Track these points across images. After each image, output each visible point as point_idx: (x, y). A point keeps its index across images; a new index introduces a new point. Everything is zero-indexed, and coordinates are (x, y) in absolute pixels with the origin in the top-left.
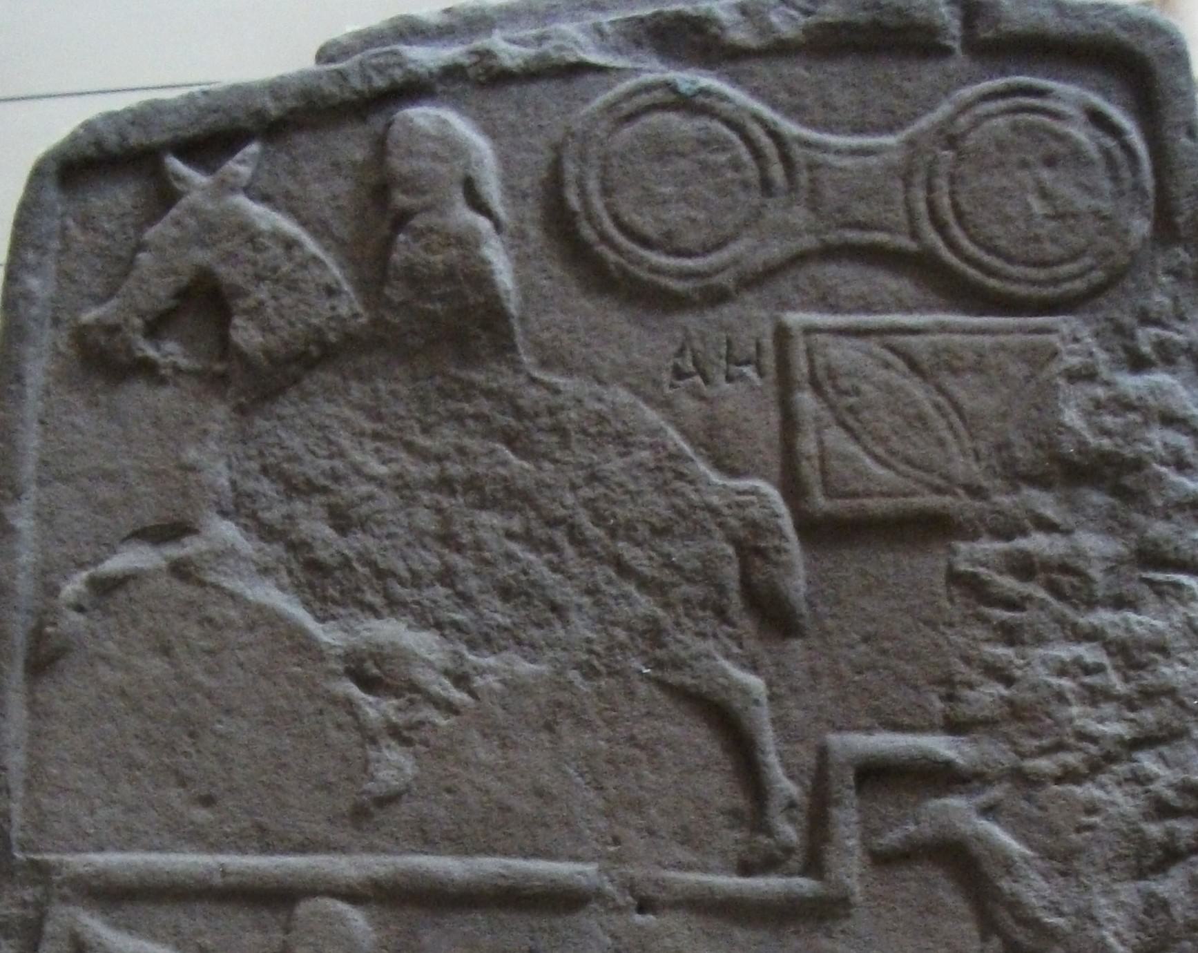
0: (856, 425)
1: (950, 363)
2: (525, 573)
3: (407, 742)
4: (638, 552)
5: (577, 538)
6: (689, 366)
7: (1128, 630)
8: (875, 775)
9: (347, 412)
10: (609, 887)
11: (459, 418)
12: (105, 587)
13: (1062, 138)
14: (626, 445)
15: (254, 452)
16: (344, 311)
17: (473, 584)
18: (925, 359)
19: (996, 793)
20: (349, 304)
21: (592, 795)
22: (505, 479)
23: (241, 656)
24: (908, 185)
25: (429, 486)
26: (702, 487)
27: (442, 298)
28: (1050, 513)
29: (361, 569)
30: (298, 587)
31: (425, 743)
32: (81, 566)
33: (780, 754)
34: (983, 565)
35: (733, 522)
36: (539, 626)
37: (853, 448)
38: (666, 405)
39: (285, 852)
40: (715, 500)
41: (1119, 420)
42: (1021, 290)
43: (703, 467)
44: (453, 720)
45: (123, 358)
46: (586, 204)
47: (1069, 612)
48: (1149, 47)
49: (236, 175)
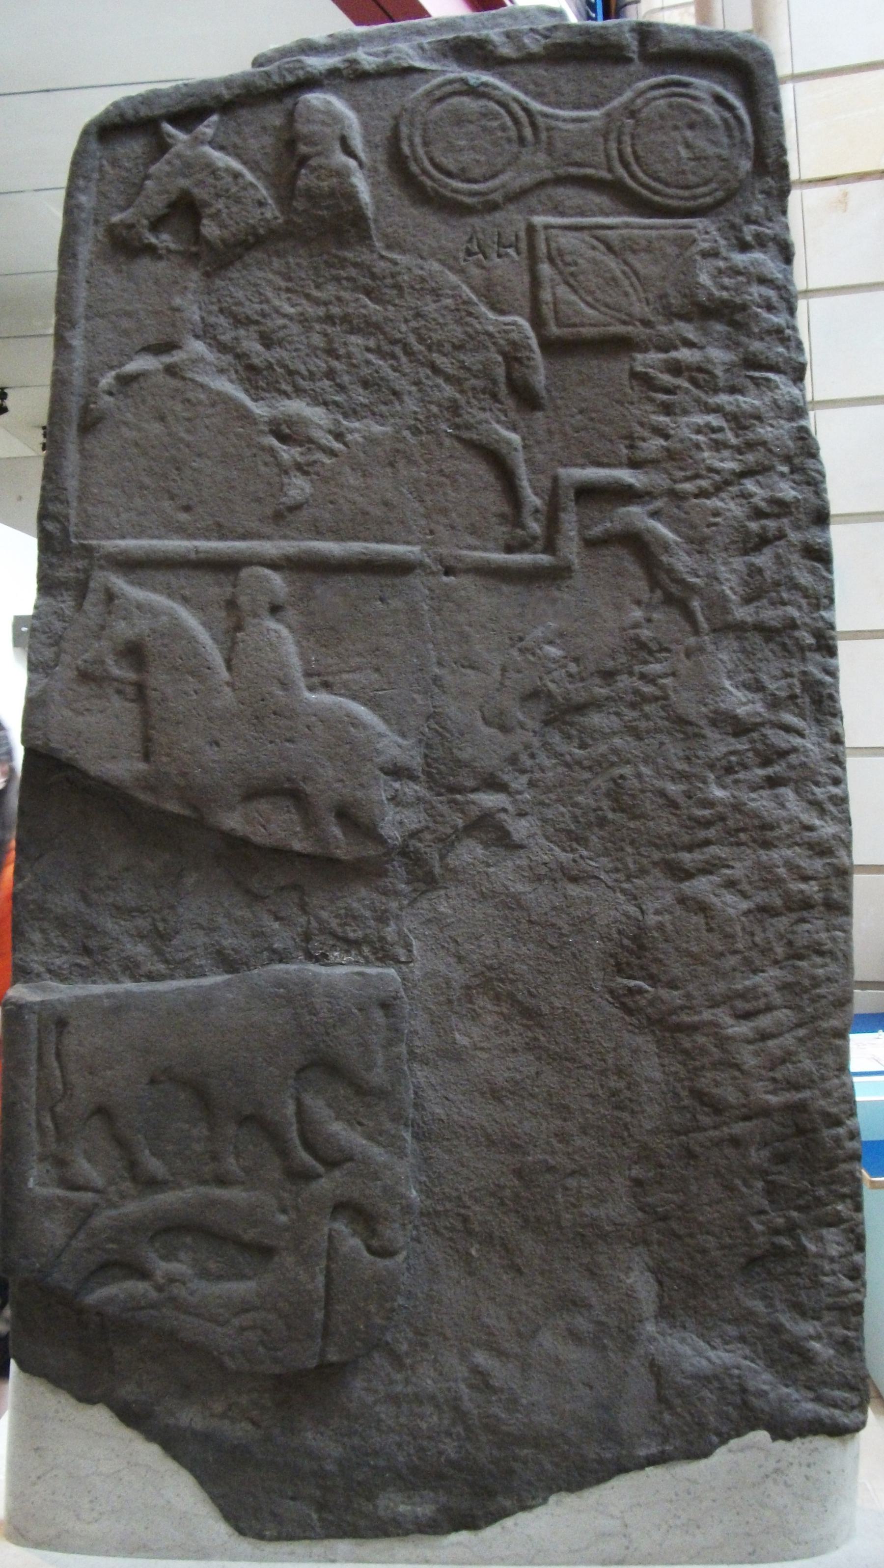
3: (306, 473)
4: (444, 359)
6: (475, 248)
7: (738, 406)
8: (587, 493)
9: (271, 276)
10: (427, 560)
11: (337, 279)
12: (126, 381)
13: (698, 112)
16: (269, 215)
17: (346, 379)
19: (659, 504)
20: (272, 211)
21: (417, 505)
23: (207, 421)
24: (606, 140)
25: (320, 320)
27: (327, 208)
28: (691, 336)
30: (241, 381)
31: (318, 474)
32: (112, 368)
33: (530, 480)
34: (652, 367)
35: (502, 342)
36: (385, 404)
37: (573, 298)
38: (461, 272)
40: (491, 328)
43: (483, 309)
44: (334, 460)
45: (136, 243)
46: (414, 151)
47: (703, 395)
48: (750, 57)
49: (204, 134)
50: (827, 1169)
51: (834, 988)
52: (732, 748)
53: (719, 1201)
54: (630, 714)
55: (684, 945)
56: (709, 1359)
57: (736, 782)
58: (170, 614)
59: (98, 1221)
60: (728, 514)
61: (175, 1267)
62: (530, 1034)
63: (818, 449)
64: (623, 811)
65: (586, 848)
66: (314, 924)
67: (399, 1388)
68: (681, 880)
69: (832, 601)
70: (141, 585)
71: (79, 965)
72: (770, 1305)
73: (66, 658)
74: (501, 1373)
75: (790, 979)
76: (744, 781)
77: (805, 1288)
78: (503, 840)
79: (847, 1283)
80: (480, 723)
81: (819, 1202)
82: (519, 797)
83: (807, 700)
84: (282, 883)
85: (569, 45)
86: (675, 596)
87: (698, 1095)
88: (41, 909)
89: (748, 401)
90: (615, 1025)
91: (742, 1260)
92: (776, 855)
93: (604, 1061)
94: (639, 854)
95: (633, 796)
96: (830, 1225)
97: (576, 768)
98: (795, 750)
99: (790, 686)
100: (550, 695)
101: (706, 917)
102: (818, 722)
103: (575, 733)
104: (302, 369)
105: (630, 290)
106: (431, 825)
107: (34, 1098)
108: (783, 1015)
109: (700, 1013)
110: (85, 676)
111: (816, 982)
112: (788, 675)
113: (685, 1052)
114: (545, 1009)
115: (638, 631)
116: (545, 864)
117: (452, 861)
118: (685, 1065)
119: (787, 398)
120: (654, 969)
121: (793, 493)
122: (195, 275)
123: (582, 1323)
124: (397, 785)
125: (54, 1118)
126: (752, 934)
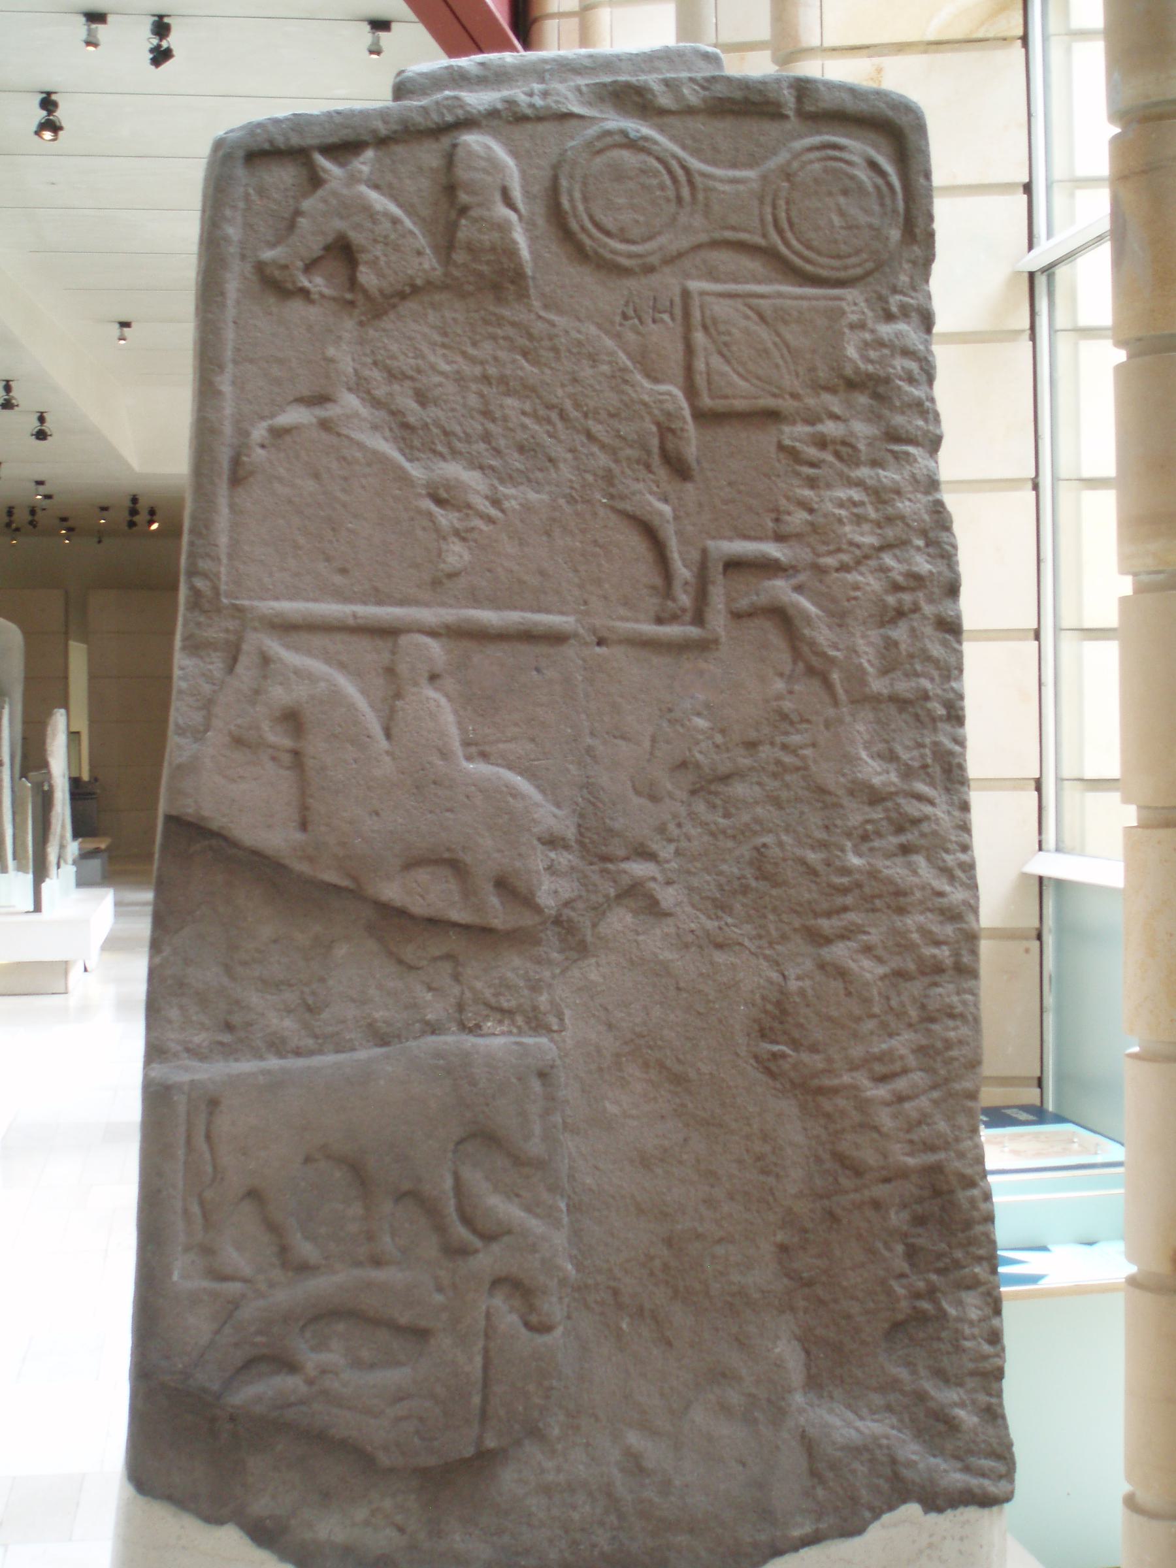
0: (728, 354)
1: (782, 316)
2: (533, 437)
3: (464, 539)
4: (600, 427)
5: (563, 415)
6: (631, 313)
7: (879, 481)
8: (734, 565)
9: (426, 330)
10: (581, 631)
11: (494, 338)
12: (278, 433)
13: (852, 178)
14: (594, 361)
15: (368, 352)
16: (426, 266)
17: (502, 442)
18: (768, 313)
19: (802, 577)
20: (429, 264)
21: (571, 575)
22: (522, 378)
23: (364, 481)
24: (762, 203)
25: (475, 379)
26: (638, 389)
27: (488, 263)
28: (836, 410)
29: (435, 430)
30: (395, 439)
31: (475, 541)
32: (263, 418)
33: (680, 553)
34: (800, 441)
35: (656, 412)
36: (541, 470)
37: (727, 368)
38: (618, 336)
39: (391, 605)
40: (646, 398)
41: (878, 353)
42: (825, 273)
43: (639, 377)
44: (491, 527)
45: (290, 286)
46: (574, 208)
47: (846, 469)
48: (903, 120)
49: (360, 172)
50: (963, 1231)
51: (965, 1050)
52: (867, 817)
53: (863, 1265)
54: (772, 784)
55: (824, 1010)
56: (857, 1430)
57: (871, 849)
58: (328, 680)
59: (247, 1312)
60: (868, 588)
61: (325, 1357)
62: (678, 1100)
63: (951, 522)
64: (765, 878)
65: (731, 915)
66: (468, 994)
67: (550, 1477)
68: (820, 945)
69: (961, 671)
70: (297, 649)
71: (221, 1044)
72: (914, 1372)
73: (217, 723)
74: (654, 1452)
75: (924, 1042)
76: (880, 849)
77: (948, 1353)
78: (653, 909)
79: (987, 1348)
80: (630, 793)
81: (957, 1265)
82: (667, 866)
83: (938, 769)
84: (437, 953)
85: (730, 100)
86: (815, 668)
87: (840, 1158)
88: (181, 985)
89: (889, 476)
90: (759, 1090)
91: (886, 1326)
92: (912, 921)
93: (749, 1125)
94: (781, 921)
95: (776, 864)
96: (969, 1288)
97: (721, 837)
98: (927, 818)
99: (923, 756)
100: (698, 766)
101: (845, 982)
102: (948, 790)
103: (718, 802)
104: (458, 429)
105: (781, 362)
106: (584, 894)
107: (180, 1184)
108: (918, 1077)
109: (841, 1076)
110: (238, 742)
111: (948, 1044)
112: (921, 745)
113: (828, 1116)
114: (692, 1074)
115: (781, 703)
116: (692, 931)
117: (603, 929)
118: (826, 1128)
119: (925, 471)
120: (796, 1034)
121: (928, 567)
122: (349, 324)
123: (734, 1398)
124: (553, 855)
125: (202, 1204)
126: (888, 998)
